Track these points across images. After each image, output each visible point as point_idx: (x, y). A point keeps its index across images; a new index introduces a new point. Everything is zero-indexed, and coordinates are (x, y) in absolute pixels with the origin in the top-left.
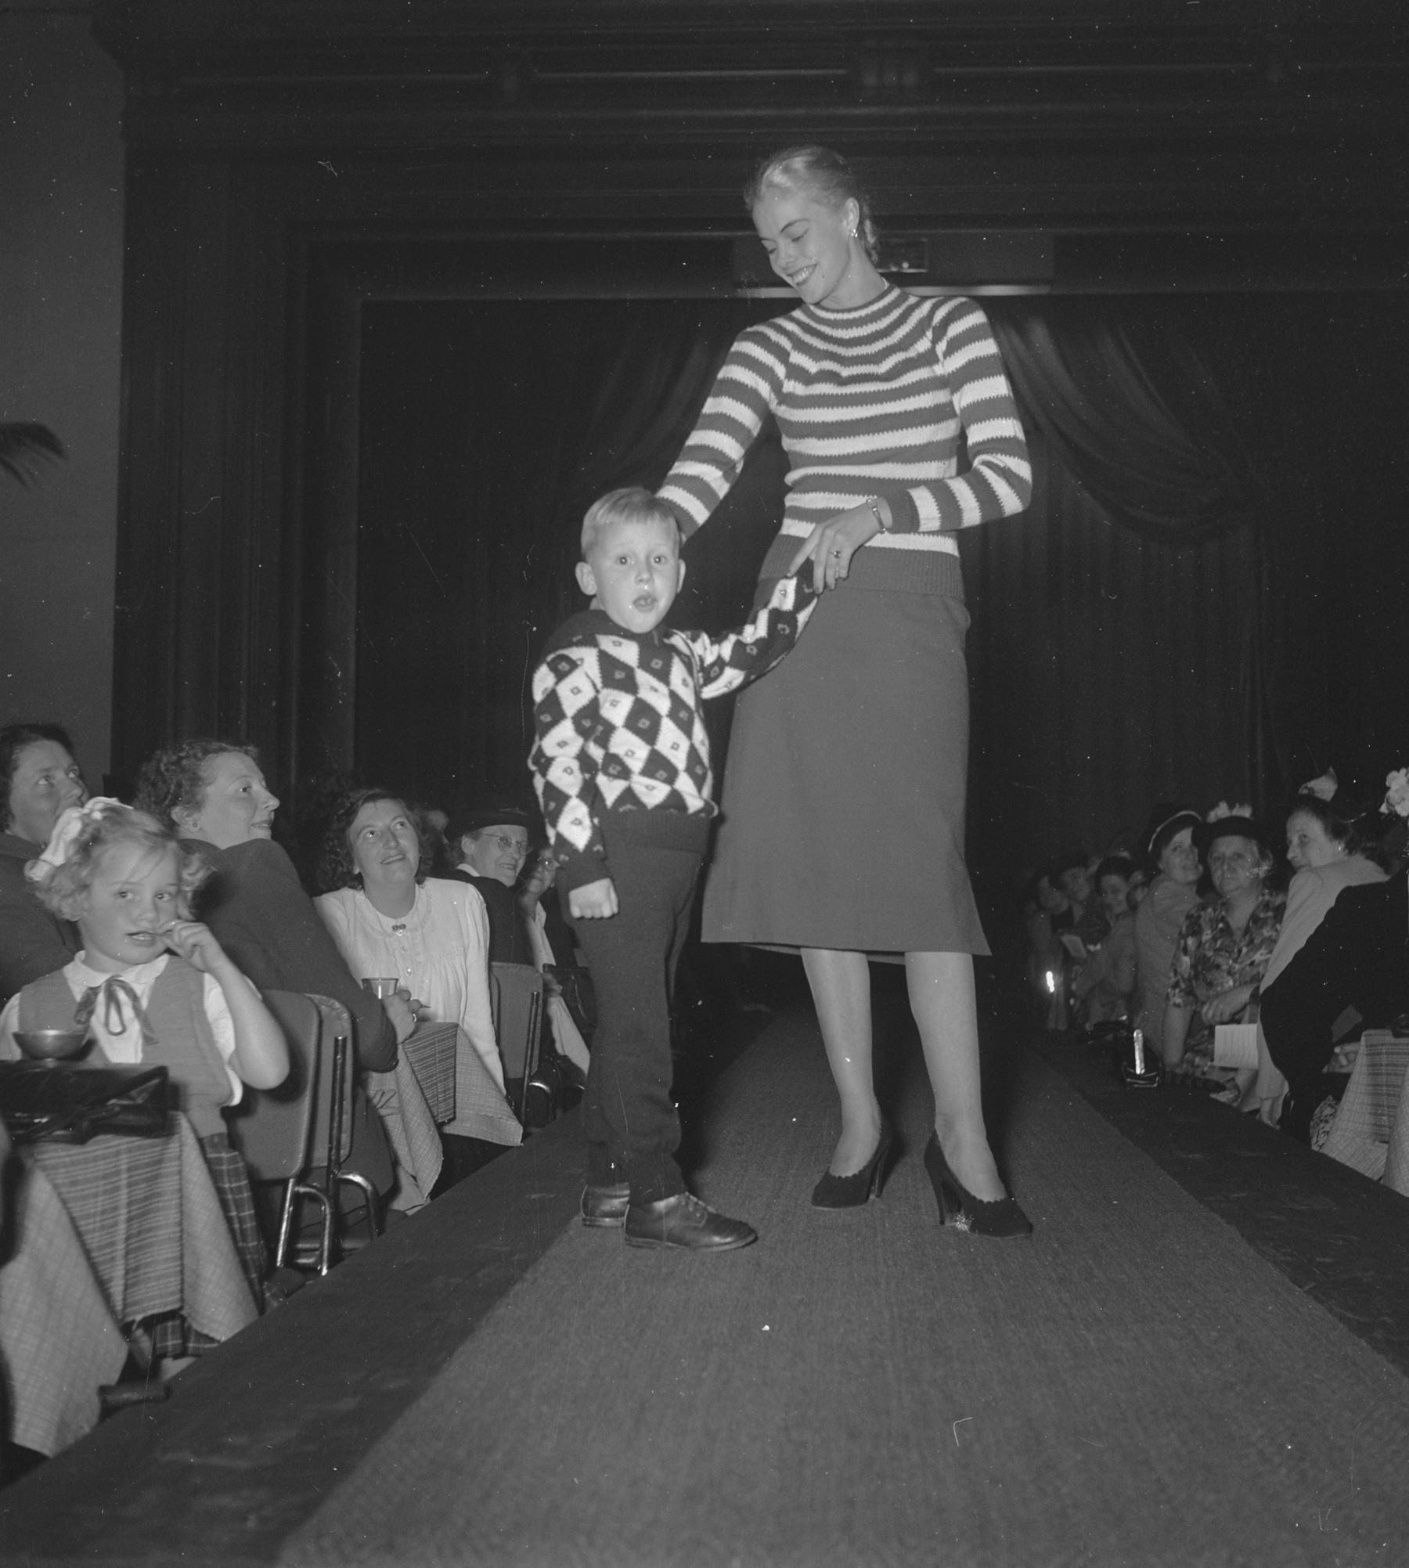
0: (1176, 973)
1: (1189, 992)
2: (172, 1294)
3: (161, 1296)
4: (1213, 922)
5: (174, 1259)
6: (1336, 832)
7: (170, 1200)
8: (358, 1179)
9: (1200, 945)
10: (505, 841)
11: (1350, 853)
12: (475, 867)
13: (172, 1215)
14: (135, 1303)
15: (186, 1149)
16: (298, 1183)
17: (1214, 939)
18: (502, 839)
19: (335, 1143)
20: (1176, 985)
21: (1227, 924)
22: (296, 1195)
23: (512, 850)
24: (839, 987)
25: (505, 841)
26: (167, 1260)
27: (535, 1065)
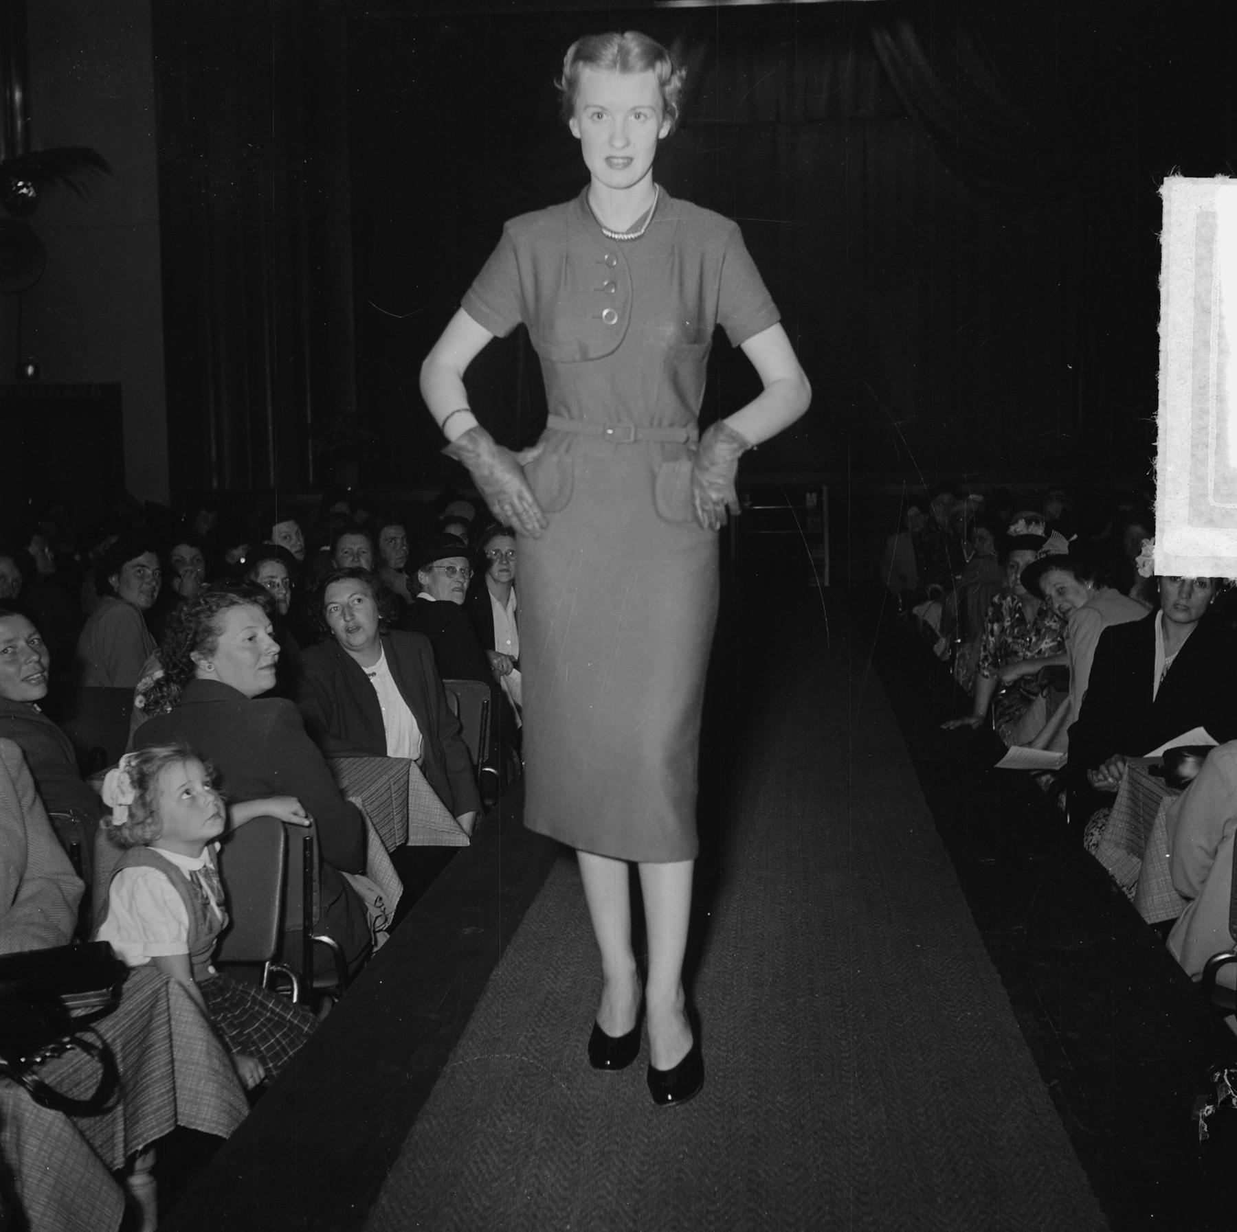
0: (985, 649)
1: (995, 665)
2: (168, 1120)
3: (158, 1125)
4: (1013, 611)
5: (168, 1092)
6: (1081, 577)
7: (160, 1046)
8: (325, 939)
9: (1003, 630)
10: (451, 569)
11: (1098, 588)
12: (431, 595)
13: (164, 1058)
14: (136, 1138)
15: (173, 998)
16: (271, 964)
17: (1012, 627)
18: (448, 568)
19: (308, 915)
20: (986, 658)
21: (1022, 614)
22: (270, 972)
23: (457, 576)
24: (603, 881)
25: (451, 569)
26: (162, 1095)
27: (486, 754)
